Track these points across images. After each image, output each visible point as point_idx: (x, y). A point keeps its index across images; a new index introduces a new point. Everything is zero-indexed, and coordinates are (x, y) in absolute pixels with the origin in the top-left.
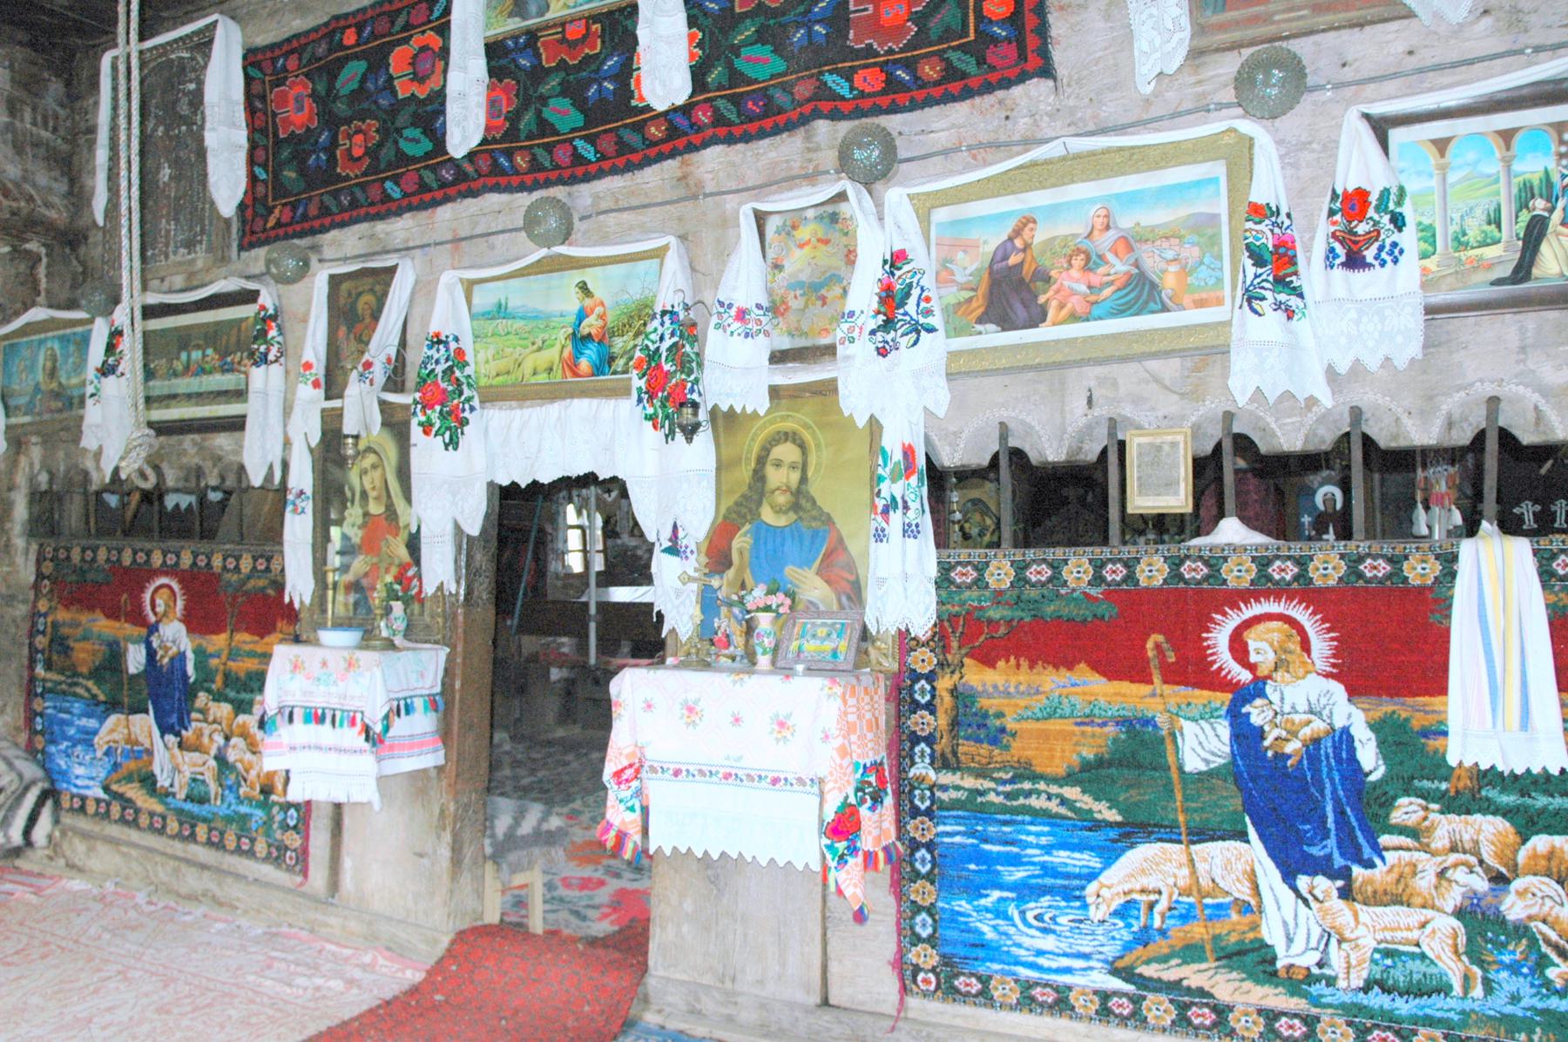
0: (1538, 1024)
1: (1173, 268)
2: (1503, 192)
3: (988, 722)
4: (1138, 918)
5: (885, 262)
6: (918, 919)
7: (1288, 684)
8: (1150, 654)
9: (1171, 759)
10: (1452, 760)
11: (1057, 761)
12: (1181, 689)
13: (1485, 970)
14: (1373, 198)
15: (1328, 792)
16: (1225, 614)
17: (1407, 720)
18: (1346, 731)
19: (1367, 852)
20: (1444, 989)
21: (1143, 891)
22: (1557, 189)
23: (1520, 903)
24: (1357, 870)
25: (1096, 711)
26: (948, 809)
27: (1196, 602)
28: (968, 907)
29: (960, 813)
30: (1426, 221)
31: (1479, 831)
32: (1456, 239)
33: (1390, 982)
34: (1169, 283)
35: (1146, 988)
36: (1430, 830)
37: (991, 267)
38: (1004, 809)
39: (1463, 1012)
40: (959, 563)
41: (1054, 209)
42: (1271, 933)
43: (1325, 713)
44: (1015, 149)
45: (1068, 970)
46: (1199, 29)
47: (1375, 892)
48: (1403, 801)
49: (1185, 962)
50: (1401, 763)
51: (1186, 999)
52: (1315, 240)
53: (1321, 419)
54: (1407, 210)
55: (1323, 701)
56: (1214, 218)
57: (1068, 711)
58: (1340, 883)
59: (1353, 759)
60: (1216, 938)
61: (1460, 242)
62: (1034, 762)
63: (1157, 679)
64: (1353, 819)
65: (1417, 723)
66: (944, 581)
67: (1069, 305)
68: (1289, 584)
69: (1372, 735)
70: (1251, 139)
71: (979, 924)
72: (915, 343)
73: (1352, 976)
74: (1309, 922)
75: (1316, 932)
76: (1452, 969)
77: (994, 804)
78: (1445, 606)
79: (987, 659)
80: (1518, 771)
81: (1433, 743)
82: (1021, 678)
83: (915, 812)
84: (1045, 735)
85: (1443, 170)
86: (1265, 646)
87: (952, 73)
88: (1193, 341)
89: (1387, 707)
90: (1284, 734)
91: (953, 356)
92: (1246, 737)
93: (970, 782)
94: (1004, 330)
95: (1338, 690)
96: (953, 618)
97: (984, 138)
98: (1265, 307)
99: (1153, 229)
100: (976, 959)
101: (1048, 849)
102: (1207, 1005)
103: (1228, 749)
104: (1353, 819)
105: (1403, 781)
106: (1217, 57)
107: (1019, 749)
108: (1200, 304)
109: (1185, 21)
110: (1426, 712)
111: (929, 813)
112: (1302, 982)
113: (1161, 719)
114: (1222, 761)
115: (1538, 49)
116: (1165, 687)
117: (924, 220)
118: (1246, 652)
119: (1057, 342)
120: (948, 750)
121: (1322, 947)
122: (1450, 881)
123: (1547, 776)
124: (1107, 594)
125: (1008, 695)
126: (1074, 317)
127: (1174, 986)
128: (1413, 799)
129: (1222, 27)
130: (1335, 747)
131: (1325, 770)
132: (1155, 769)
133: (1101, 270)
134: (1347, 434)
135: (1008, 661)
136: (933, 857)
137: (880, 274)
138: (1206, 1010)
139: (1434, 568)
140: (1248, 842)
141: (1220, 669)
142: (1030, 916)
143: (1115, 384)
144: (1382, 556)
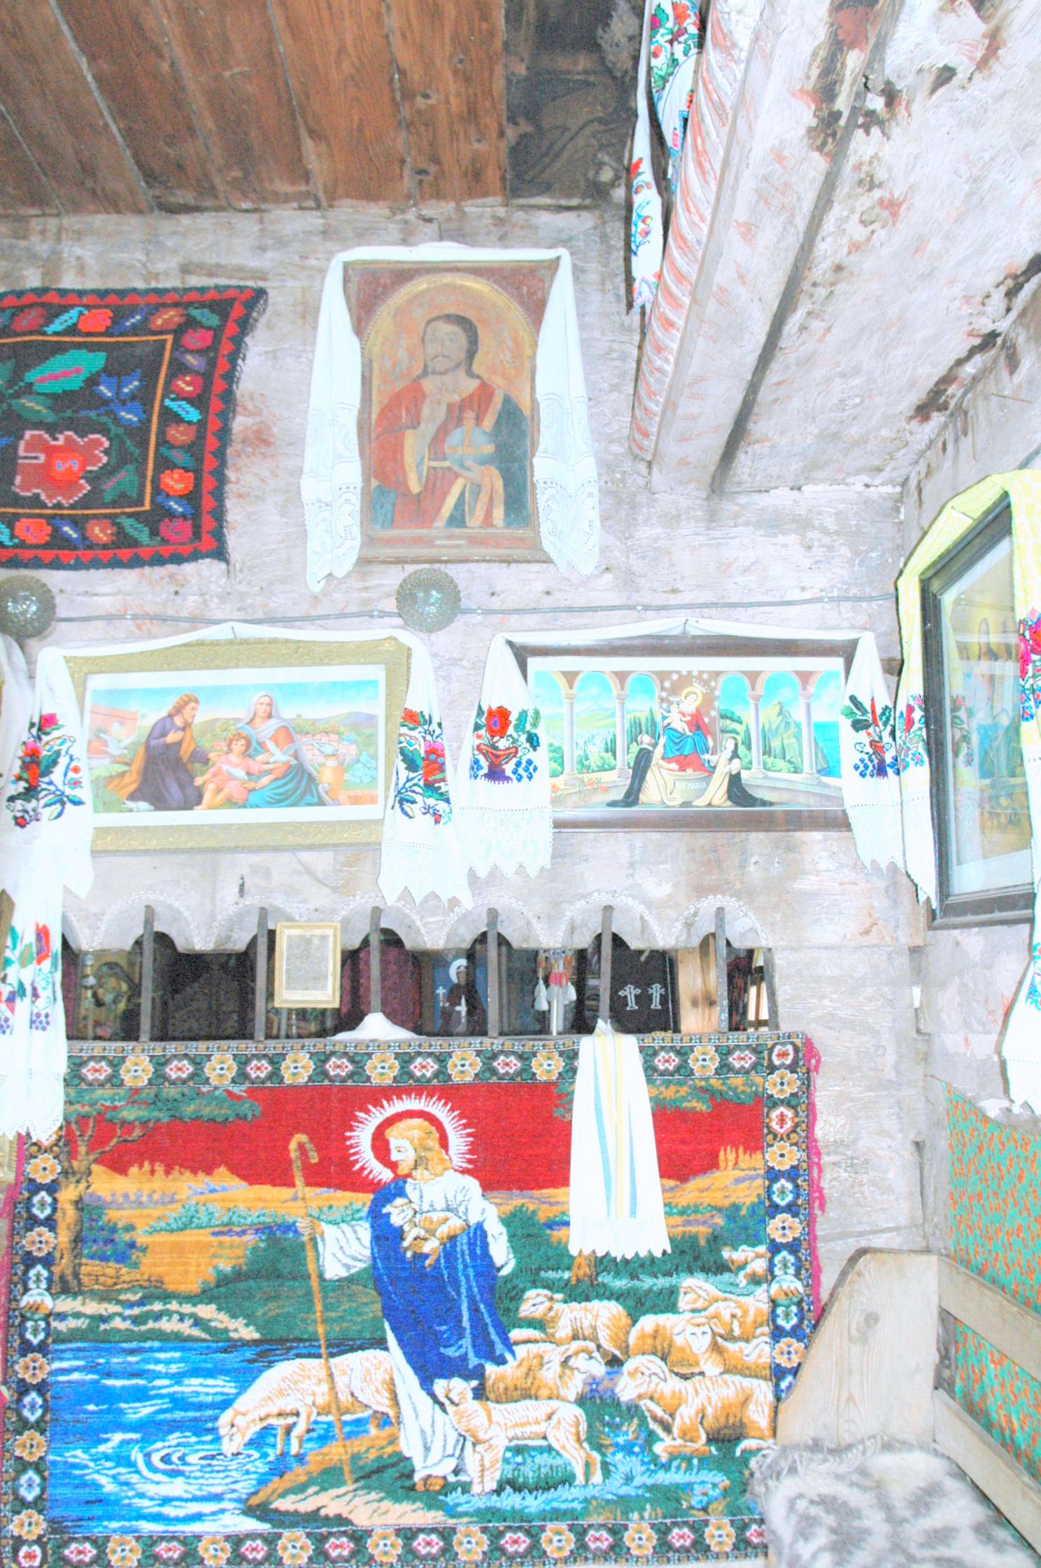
0: (648, 1500)
1: (332, 763)
2: (619, 726)
3: (116, 1237)
4: (274, 1446)
5: (32, 725)
6: (24, 1479)
7: (426, 1181)
8: (293, 1155)
9: (311, 1267)
10: (574, 1251)
11: (192, 1276)
12: (323, 1192)
13: (603, 1455)
14: (513, 718)
15: (463, 1290)
16: (367, 1112)
17: (534, 1212)
18: (480, 1226)
19: (499, 1348)
20: (568, 1480)
21: (280, 1415)
22: (660, 729)
23: (632, 1383)
24: (490, 1368)
25: (235, 1219)
26: (63, 1341)
27: (341, 1101)
28: (86, 1456)
29: (80, 1345)
30: (557, 744)
31: (596, 1317)
32: (580, 762)
33: (521, 1480)
34: (326, 778)
35: (282, 1524)
36: (554, 1320)
37: (148, 742)
38: (129, 1336)
39: (586, 1500)
40: (92, 1058)
41: (218, 692)
42: (409, 1445)
43: (462, 1209)
44: (183, 625)
45: (198, 1517)
46: (369, 540)
47: (506, 1389)
48: (531, 1293)
49: (323, 1489)
50: (530, 1255)
51: (324, 1530)
52: (462, 746)
53: (463, 919)
54: (540, 732)
55: (460, 1198)
56: (371, 719)
57: (204, 1220)
58: (474, 1383)
59: (486, 1255)
60: (355, 1457)
61: (584, 766)
62: (166, 1279)
63: (299, 1181)
64: (486, 1316)
65: (544, 1214)
66: (74, 1078)
67: (227, 790)
68: (429, 1081)
69: (504, 1230)
70: (409, 649)
71: (96, 1476)
72: (60, 815)
73: (487, 1478)
74: (445, 1427)
75: (453, 1436)
76: (575, 1456)
77: (119, 1331)
78: (566, 1099)
79: (118, 1165)
80: (629, 1257)
81: (557, 1234)
82: (156, 1185)
83: (26, 1348)
84: (179, 1249)
86: (405, 1143)
87: (122, 540)
88: (346, 837)
89: (517, 1200)
90: (422, 1233)
91: (101, 832)
92: (387, 1237)
93: (92, 1308)
94: (157, 809)
95: (473, 1184)
96: (83, 1120)
97: (150, 609)
98: (416, 809)
99: (313, 723)
100: (91, 1519)
101: (178, 1378)
102: (344, 1533)
103: (368, 1253)
104: (486, 1316)
105: (531, 1275)
106: (383, 567)
107: (149, 1266)
108: (356, 800)
109: (356, 531)
110: (551, 1204)
111: (42, 1348)
112: (439, 1493)
113: (302, 1224)
114: (362, 1265)
115: (646, 608)
116: (308, 1189)
117: (80, 686)
118: (388, 1151)
119: (213, 826)
120: (69, 1272)
121: (458, 1452)
122: (572, 1369)
123: (653, 1259)
124: (251, 1092)
125: (140, 1204)
126: (230, 803)
127: (313, 1517)
128: (540, 1291)
129: (389, 542)
130: (469, 1244)
131: (461, 1267)
132: (295, 1279)
133: (260, 758)
134: (484, 935)
135: (141, 1167)
136: (45, 1400)
137: (25, 736)
138: (344, 1540)
139: (558, 1064)
140: (386, 1349)
141: (362, 1168)
142: (156, 1458)
143: (267, 874)
144: (513, 1053)
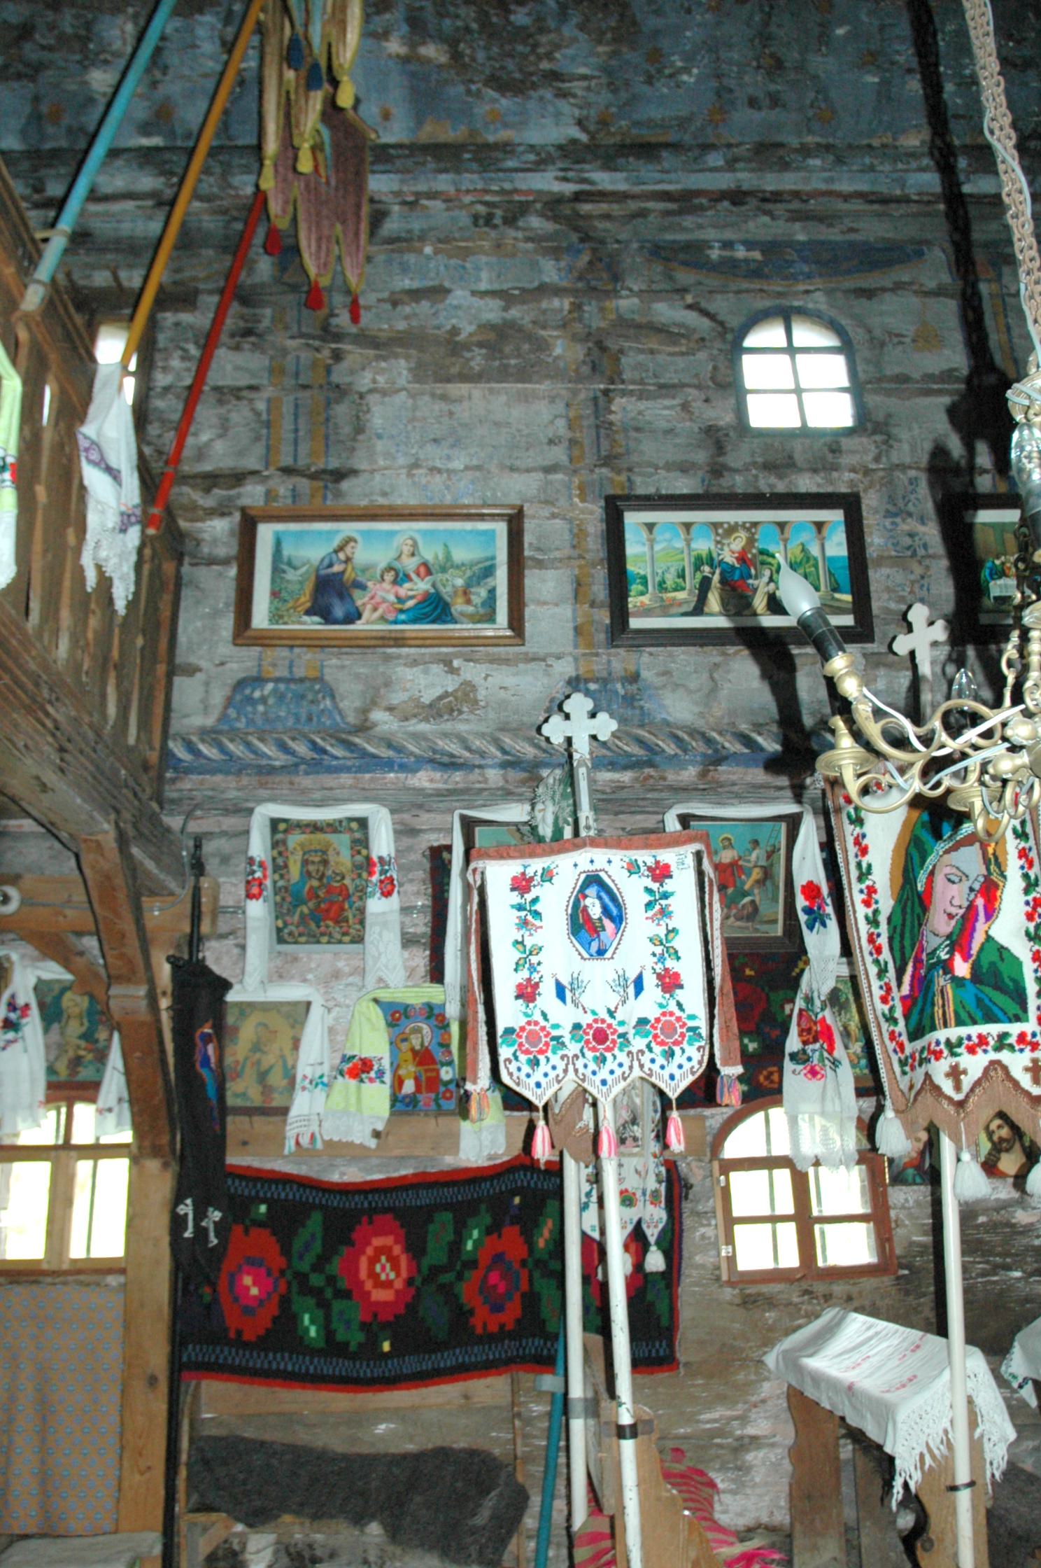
61: (662, 586)
85: (652, 542)
